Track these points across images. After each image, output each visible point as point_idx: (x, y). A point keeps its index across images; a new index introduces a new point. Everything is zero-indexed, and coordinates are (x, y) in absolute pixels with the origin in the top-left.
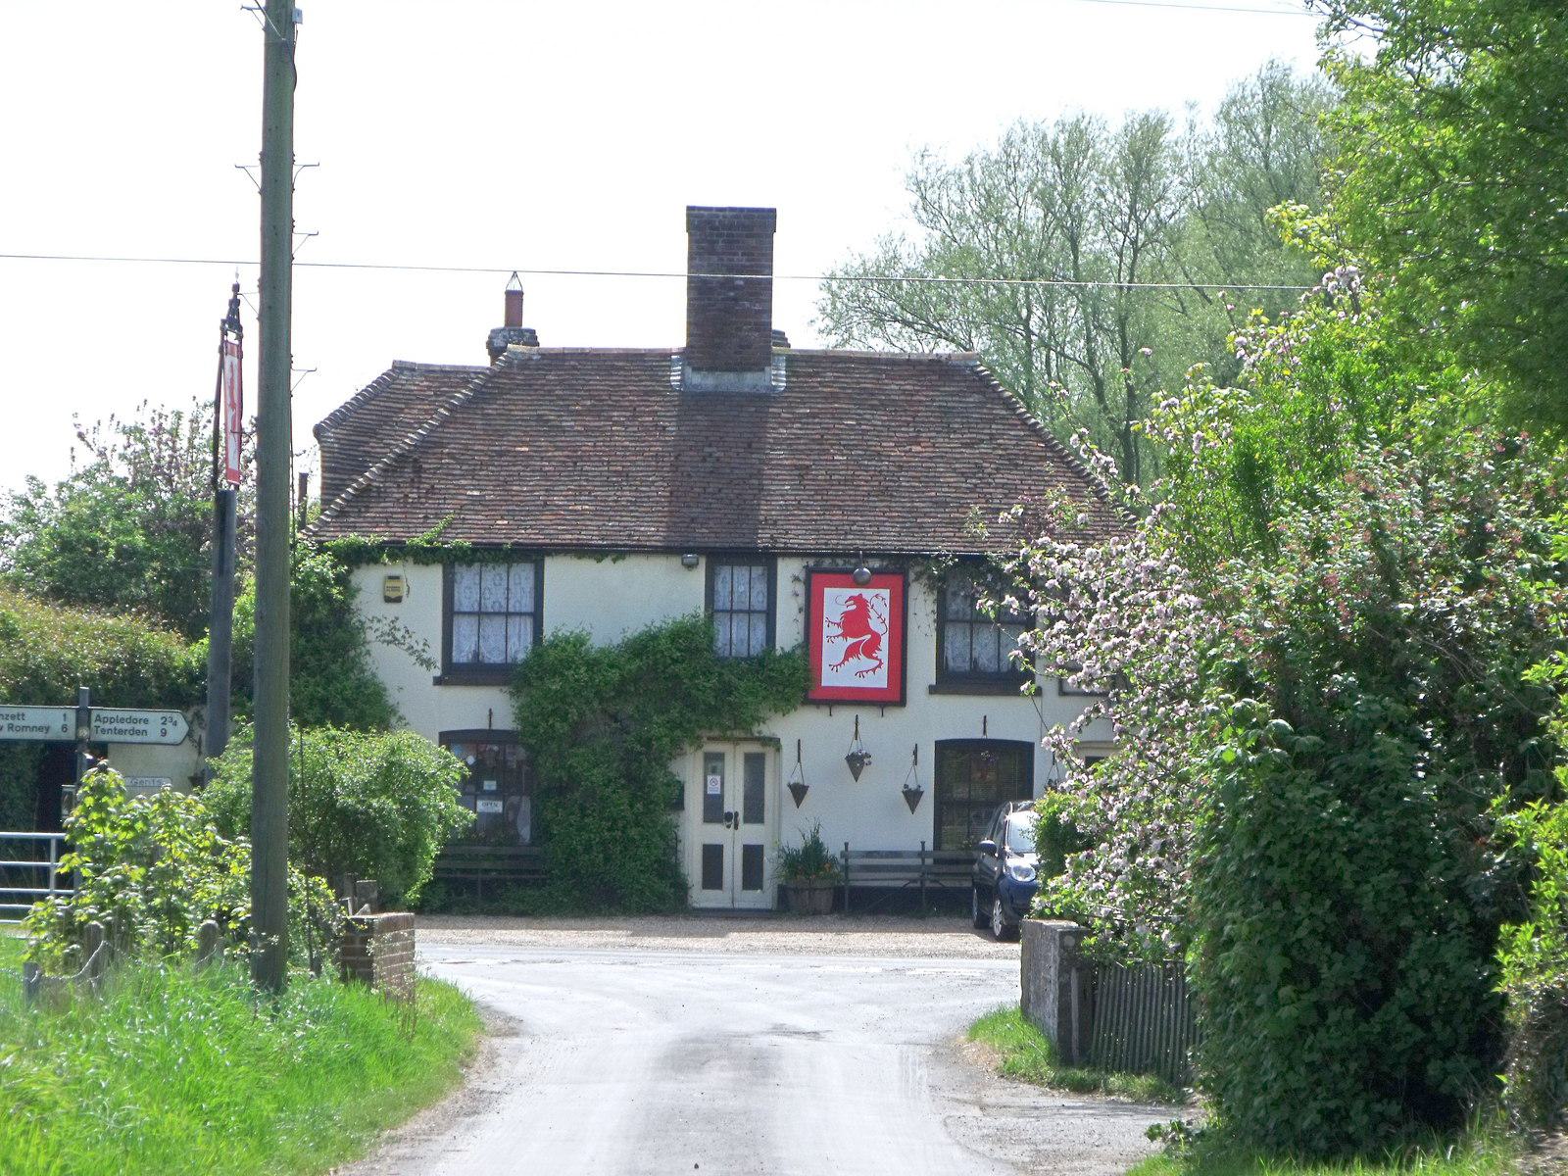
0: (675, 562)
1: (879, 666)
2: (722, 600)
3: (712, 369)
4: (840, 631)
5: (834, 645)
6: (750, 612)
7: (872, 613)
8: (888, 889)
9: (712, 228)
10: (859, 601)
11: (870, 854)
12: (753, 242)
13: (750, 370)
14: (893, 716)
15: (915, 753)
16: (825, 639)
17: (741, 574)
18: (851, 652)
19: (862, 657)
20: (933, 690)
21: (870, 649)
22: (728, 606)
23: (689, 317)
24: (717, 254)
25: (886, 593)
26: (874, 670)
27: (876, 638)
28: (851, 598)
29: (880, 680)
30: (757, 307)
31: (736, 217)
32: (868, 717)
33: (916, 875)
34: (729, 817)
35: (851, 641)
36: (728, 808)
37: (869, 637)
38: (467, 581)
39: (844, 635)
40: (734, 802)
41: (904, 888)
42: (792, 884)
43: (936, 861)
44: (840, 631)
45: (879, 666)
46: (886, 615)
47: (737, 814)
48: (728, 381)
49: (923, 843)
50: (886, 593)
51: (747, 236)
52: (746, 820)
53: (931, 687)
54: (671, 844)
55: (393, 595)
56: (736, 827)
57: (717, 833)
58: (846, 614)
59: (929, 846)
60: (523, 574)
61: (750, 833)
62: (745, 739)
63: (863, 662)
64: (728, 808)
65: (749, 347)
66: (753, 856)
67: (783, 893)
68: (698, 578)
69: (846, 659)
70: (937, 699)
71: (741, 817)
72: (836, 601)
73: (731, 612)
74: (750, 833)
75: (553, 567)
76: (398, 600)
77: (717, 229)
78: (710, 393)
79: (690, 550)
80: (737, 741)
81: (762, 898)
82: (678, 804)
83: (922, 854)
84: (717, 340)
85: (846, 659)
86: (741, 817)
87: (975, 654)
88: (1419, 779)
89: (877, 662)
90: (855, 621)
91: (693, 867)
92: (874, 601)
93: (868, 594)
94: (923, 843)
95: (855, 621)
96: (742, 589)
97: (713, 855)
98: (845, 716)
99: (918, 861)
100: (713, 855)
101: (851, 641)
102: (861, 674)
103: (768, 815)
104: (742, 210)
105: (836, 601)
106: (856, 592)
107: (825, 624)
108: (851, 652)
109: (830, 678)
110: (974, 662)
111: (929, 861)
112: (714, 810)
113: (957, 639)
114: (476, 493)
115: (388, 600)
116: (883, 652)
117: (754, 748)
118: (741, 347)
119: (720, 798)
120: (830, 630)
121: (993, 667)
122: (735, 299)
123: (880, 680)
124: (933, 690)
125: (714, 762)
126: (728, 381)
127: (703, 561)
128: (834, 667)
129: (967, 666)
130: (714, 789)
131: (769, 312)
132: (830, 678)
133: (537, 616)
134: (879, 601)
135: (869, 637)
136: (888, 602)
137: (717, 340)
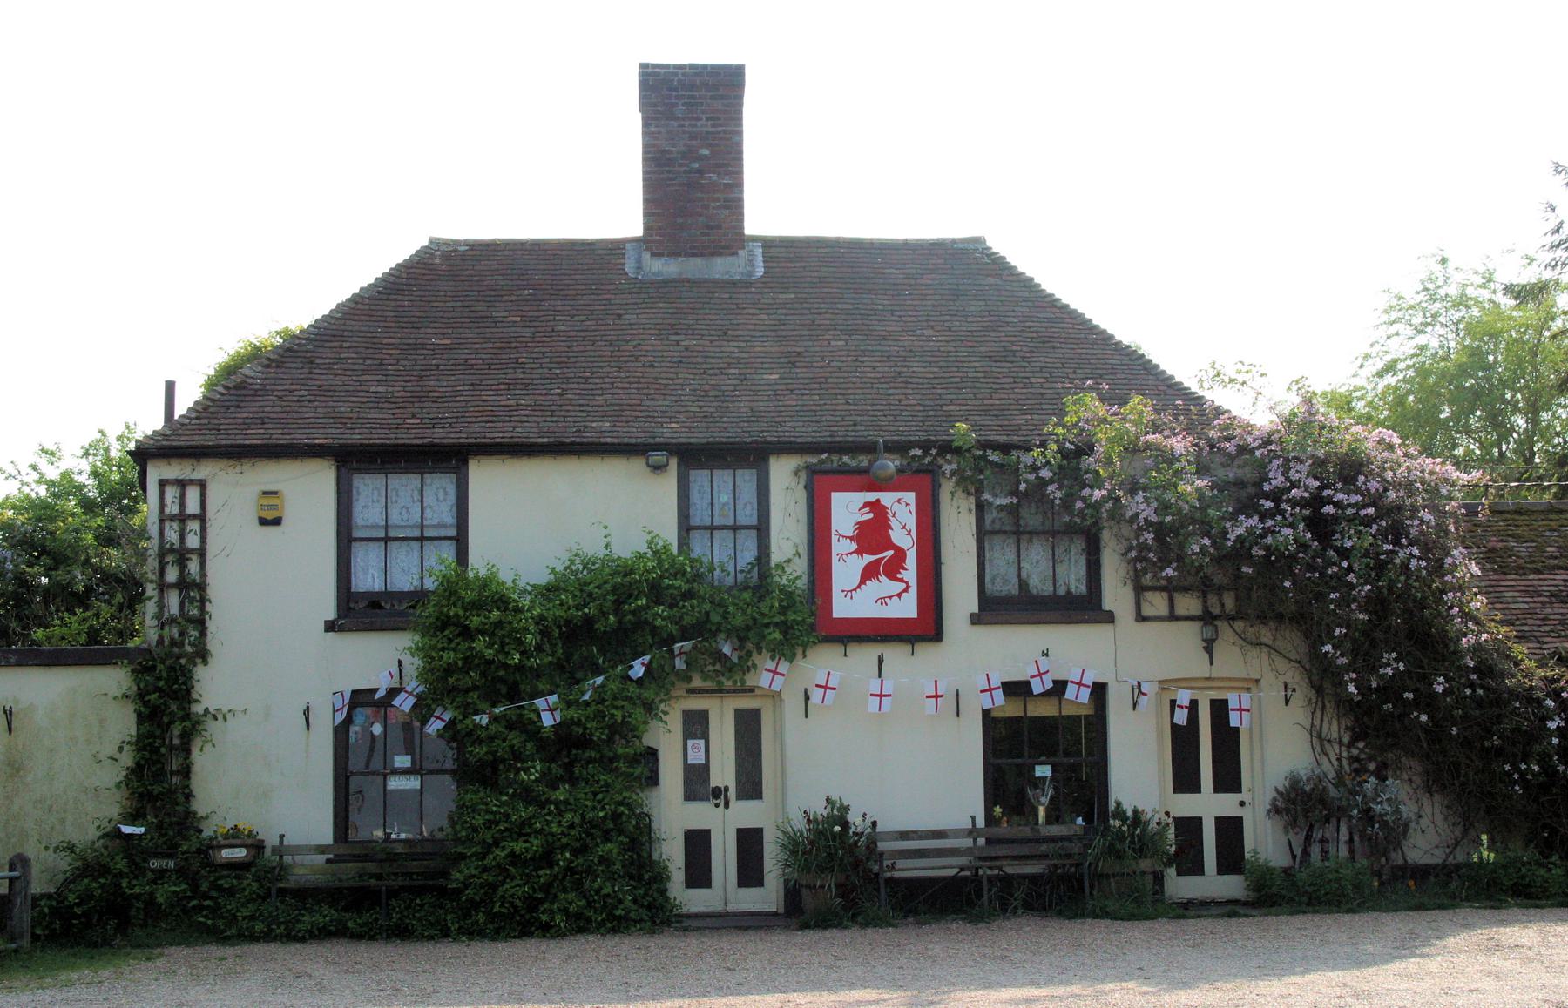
0: (637, 465)
1: (906, 590)
2: (700, 515)
3: (675, 254)
4: (854, 547)
5: (846, 567)
6: (735, 528)
7: (894, 523)
8: (932, 881)
9: (670, 89)
10: (875, 506)
11: (904, 835)
12: (719, 105)
13: (721, 254)
14: (926, 651)
15: (958, 695)
16: (835, 558)
17: (723, 478)
18: (869, 573)
19: (883, 578)
20: (976, 620)
21: (893, 569)
22: (707, 522)
23: (644, 166)
24: (677, 119)
25: (910, 497)
26: (899, 595)
27: (900, 554)
28: (866, 505)
29: (907, 608)
30: (727, 180)
31: (696, 75)
32: (895, 655)
33: (963, 861)
34: (717, 793)
35: (868, 558)
36: (715, 781)
37: (890, 553)
38: (369, 490)
39: (859, 552)
40: (724, 773)
41: (954, 878)
42: (806, 880)
43: (989, 841)
44: (854, 547)
45: (906, 590)
46: (912, 525)
47: (727, 789)
48: (693, 267)
49: (973, 818)
50: (910, 497)
51: (712, 97)
52: (742, 796)
53: (972, 615)
54: (640, 836)
55: (270, 515)
56: (727, 805)
57: (702, 815)
58: (862, 526)
59: (981, 823)
60: (440, 487)
61: (745, 814)
62: (735, 691)
63: (885, 586)
64: (715, 781)
65: (719, 227)
66: (749, 841)
67: (792, 894)
68: (665, 488)
69: (862, 582)
70: (981, 631)
71: (732, 793)
72: (847, 509)
73: (712, 528)
74: (745, 814)
75: (485, 477)
76: (277, 522)
77: (676, 90)
78: (674, 281)
79: (658, 447)
80: (720, 691)
81: (767, 897)
82: (653, 780)
83: (972, 832)
84: (680, 220)
85: (862, 582)
86: (732, 793)
87: (1024, 574)
88: (1415, 691)
89: (904, 585)
90: (873, 534)
91: (672, 853)
92: (896, 507)
93: (887, 498)
94: (973, 818)
95: (873, 534)
96: (724, 498)
97: (698, 842)
98: (864, 656)
99: (968, 842)
100: (698, 842)
101: (868, 558)
102: (882, 601)
103: (767, 790)
104: (705, 67)
105: (847, 509)
106: (871, 496)
107: (834, 539)
108: (869, 573)
109: (845, 606)
110: (1023, 584)
111: (981, 841)
112: (697, 783)
113: (1002, 558)
114: (380, 389)
115: (263, 522)
116: (910, 573)
117: (746, 703)
118: (709, 227)
119: (705, 768)
120: (841, 546)
121: (1047, 589)
122: (700, 171)
123: (907, 608)
124: (976, 620)
125: (696, 725)
126: (693, 267)
127: (674, 463)
128: (849, 593)
129: (1015, 591)
130: (696, 757)
131: (742, 221)
132: (845, 606)
133: (461, 540)
134: (902, 509)
135: (890, 553)
136: (913, 508)
137: (680, 220)
